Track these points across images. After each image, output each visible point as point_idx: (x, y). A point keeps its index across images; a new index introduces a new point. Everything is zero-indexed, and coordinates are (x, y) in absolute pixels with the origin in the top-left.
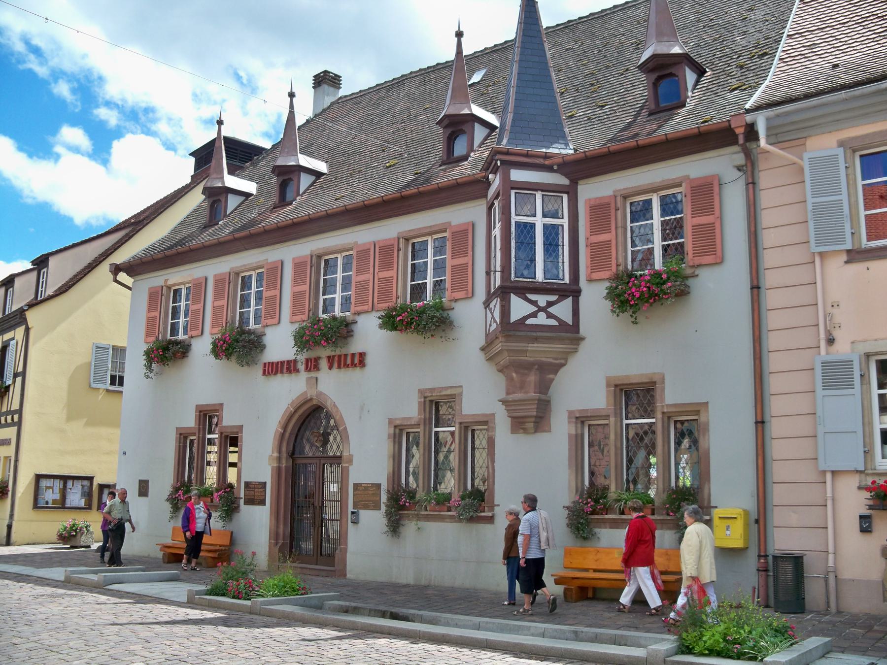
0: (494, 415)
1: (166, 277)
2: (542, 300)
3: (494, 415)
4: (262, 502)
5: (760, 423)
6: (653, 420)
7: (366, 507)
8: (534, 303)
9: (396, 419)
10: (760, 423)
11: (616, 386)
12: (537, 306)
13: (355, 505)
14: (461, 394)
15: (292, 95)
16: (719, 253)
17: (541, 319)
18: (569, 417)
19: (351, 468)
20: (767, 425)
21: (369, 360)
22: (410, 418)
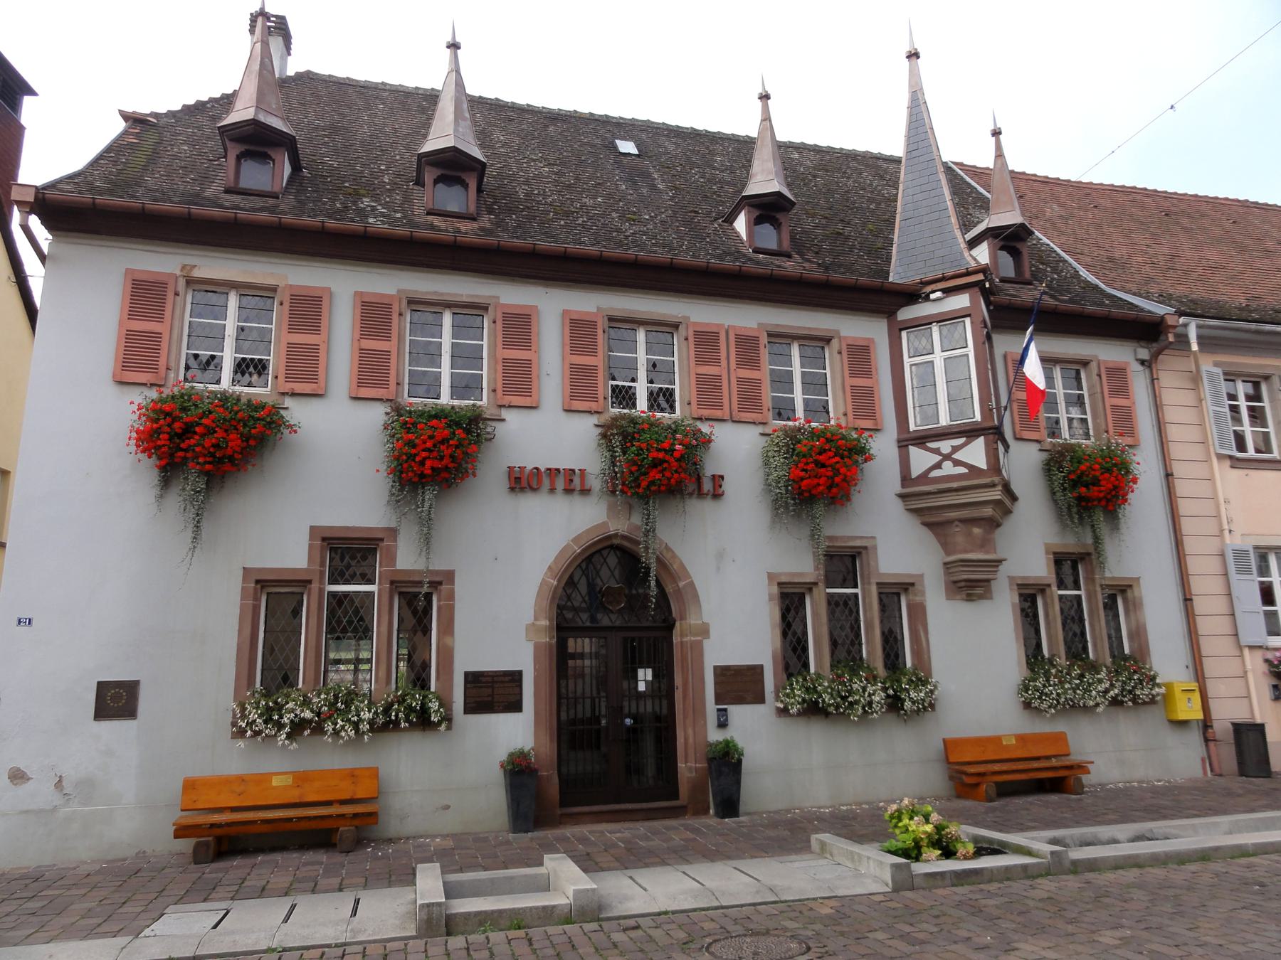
0: (922, 576)
1: (189, 260)
2: (945, 446)
3: (922, 576)
4: (516, 707)
5: (1187, 600)
6: (829, 590)
7: (740, 700)
8: (937, 451)
9: (780, 574)
10: (1187, 600)
11: (324, 539)
12: (940, 454)
13: (719, 699)
14: (875, 547)
15: (996, 133)
16: (322, 383)
17: (948, 469)
18: (1011, 585)
19: (706, 642)
20: (1181, 598)
21: (727, 486)
22: (801, 574)
